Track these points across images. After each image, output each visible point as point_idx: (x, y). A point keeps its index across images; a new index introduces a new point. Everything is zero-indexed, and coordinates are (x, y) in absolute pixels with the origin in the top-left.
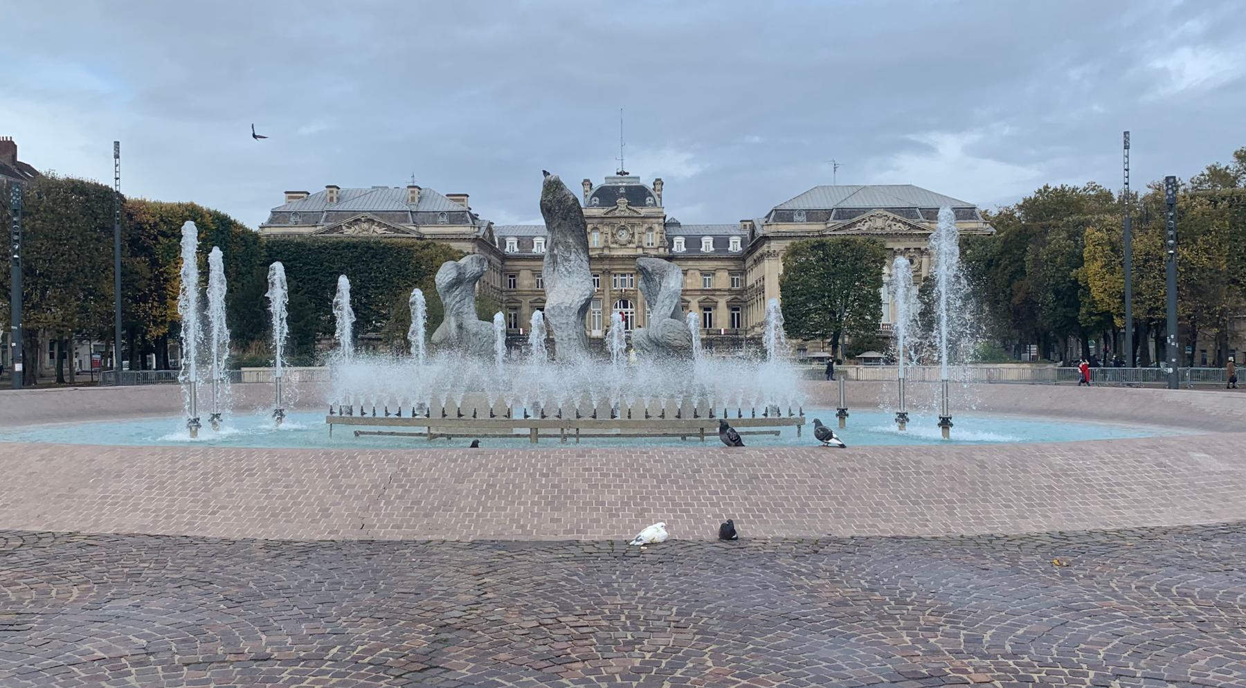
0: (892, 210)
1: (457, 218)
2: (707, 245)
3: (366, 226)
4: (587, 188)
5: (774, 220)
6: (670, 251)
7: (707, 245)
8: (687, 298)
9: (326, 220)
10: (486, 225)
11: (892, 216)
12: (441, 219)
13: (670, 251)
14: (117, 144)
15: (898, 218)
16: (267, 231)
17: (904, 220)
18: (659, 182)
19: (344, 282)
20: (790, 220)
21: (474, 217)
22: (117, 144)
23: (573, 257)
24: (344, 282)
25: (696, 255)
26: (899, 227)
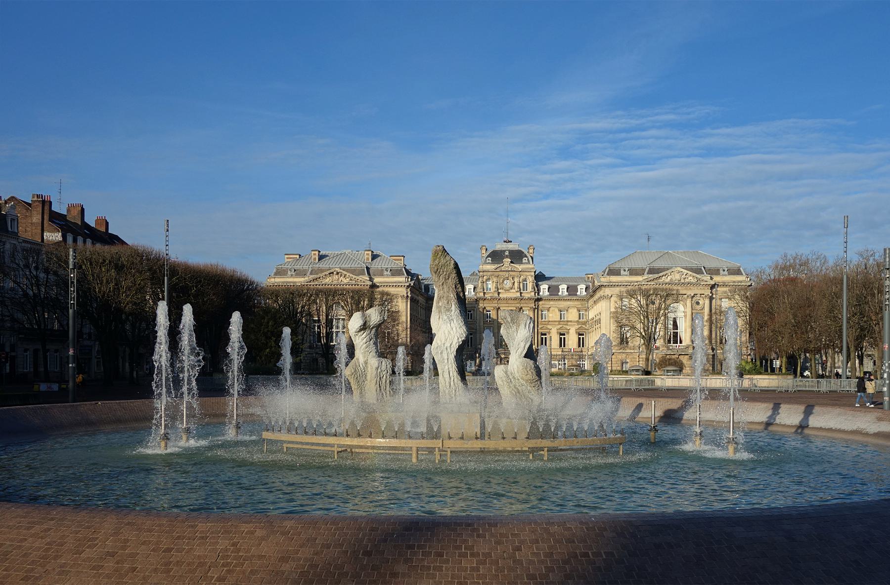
4: (484, 251)
9: (311, 274)
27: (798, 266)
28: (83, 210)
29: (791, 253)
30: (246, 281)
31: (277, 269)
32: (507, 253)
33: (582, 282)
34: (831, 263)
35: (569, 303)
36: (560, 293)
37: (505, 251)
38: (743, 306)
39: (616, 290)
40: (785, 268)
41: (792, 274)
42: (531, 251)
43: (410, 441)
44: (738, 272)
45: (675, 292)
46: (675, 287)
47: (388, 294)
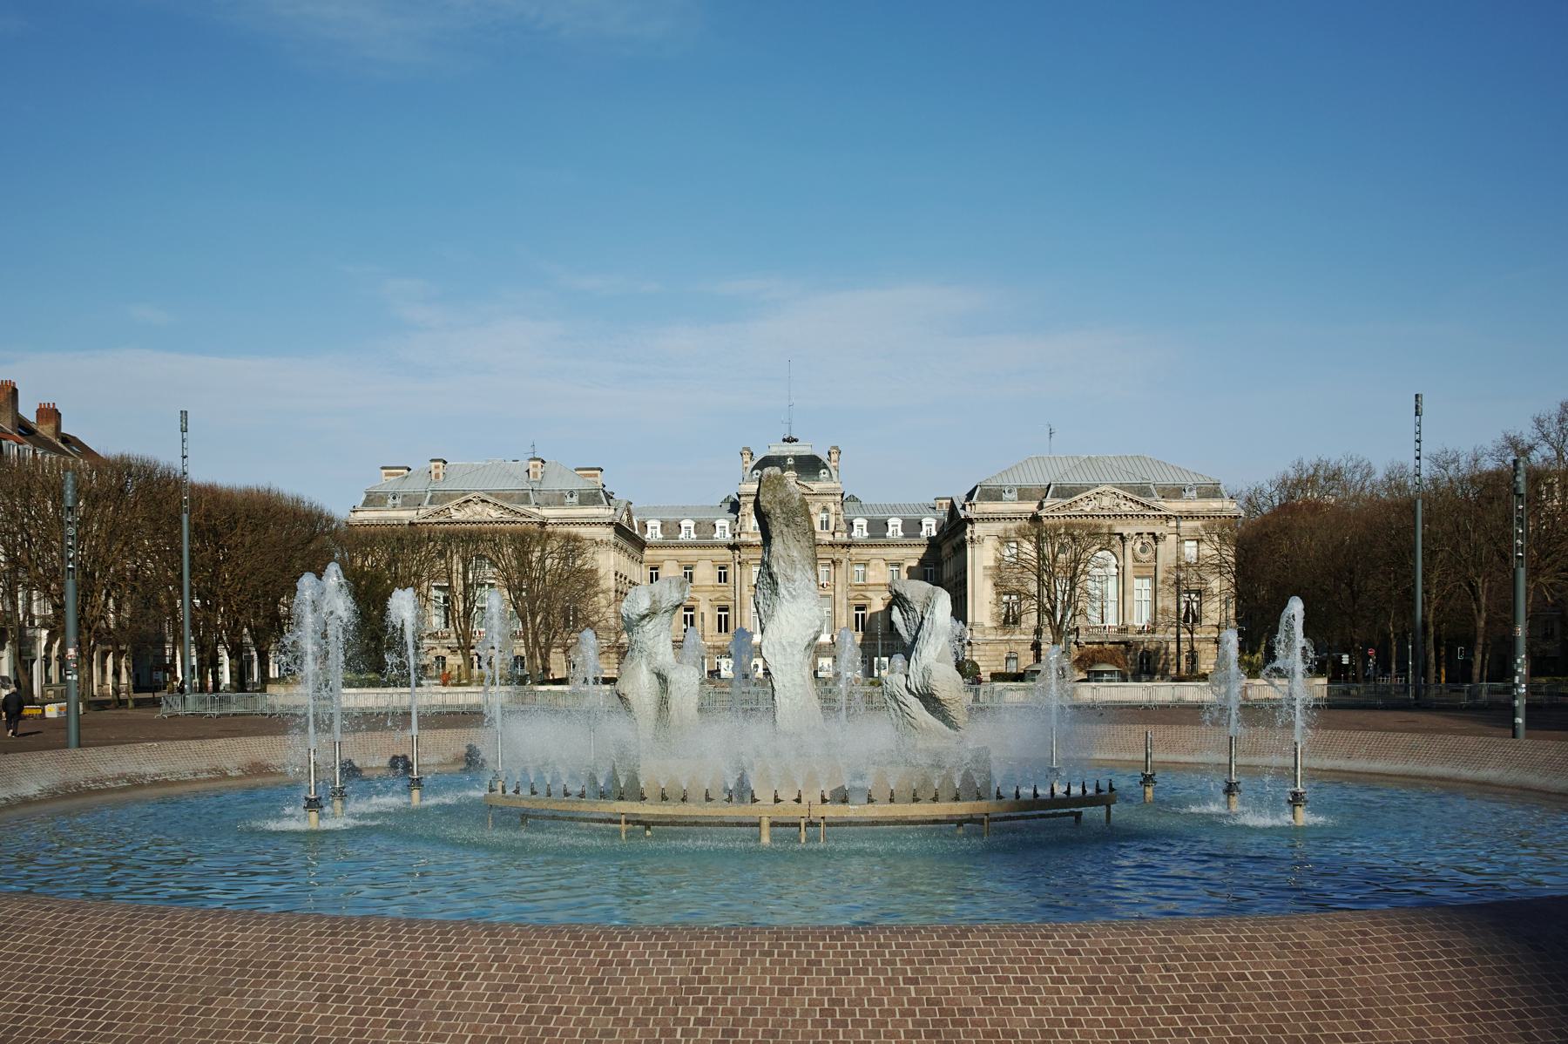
0: (1121, 487)
1: (589, 498)
2: (895, 526)
3: (478, 508)
4: (747, 458)
5: (979, 499)
6: (849, 536)
7: (895, 526)
8: (868, 594)
9: (431, 503)
10: (623, 505)
11: (1121, 493)
12: (569, 499)
13: (849, 536)
14: (184, 414)
15: (1129, 496)
16: (360, 515)
17: (1136, 498)
19: (1296, 607)
20: (998, 498)
21: (609, 497)
22: (184, 414)
23: (797, 576)
24: (1296, 607)
25: (881, 541)
26: (1127, 507)
27: (1321, 481)
28: (15, 391)
29: (1309, 460)
30: (320, 516)
31: (369, 495)
32: (790, 462)
33: (686, 516)
34: (1379, 475)
35: (905, 551)
36: (889, 534)
37: (785, 458)
38: (1229, 554)
39: (998, 527)
40: (1300, 484)
41: (1311, 495)
42: (834, 457)
43: (621, 803)
44: (1213, 492)
45: (1105, 530)
46: (1108, 522)
47: (576, 538)
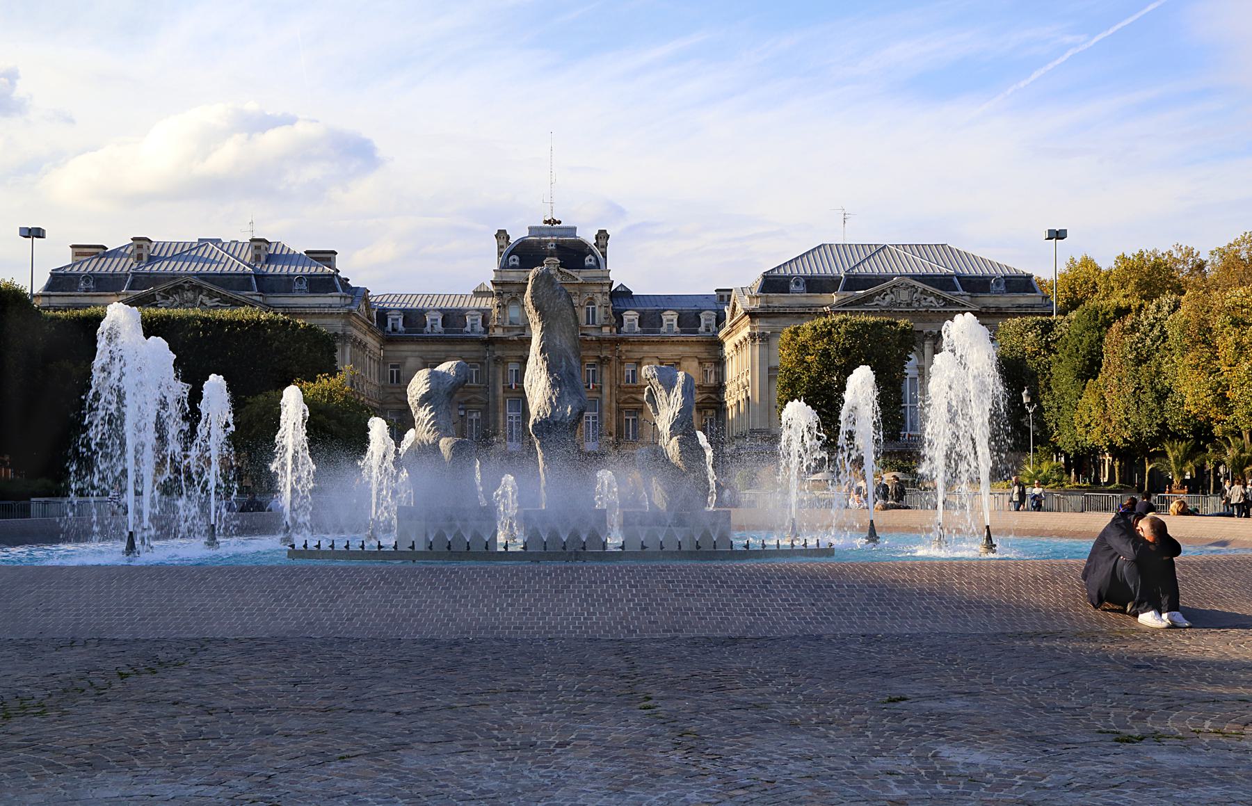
18: (602, 236)
